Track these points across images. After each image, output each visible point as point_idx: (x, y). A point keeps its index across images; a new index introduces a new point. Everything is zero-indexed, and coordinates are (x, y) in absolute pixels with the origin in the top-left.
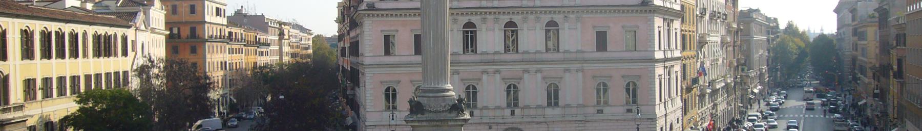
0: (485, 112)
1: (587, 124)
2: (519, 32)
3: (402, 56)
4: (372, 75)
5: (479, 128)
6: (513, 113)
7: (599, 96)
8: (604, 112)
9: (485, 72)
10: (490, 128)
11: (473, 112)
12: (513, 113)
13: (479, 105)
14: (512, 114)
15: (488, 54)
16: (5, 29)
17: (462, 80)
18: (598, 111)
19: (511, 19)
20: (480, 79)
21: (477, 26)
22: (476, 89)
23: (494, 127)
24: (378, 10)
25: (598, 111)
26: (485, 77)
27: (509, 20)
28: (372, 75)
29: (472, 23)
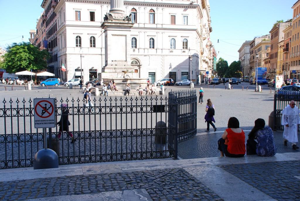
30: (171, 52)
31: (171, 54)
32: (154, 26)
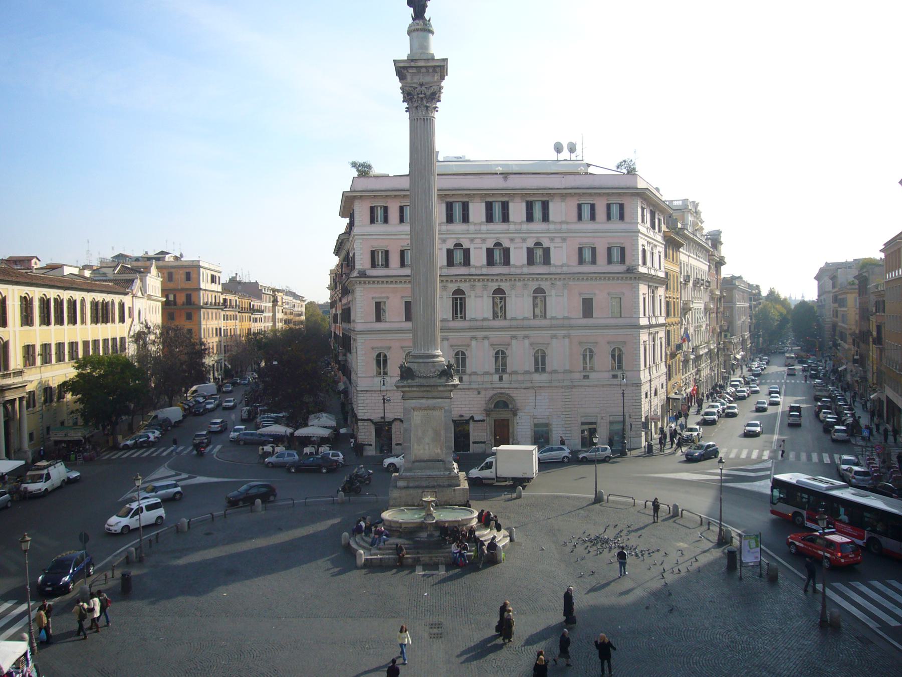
0: (474, 378)
1: (574, 390)
2: (507, 299)
4: (363, 341)
8: (590, 377)
10: (479, 393)
12: (501, 379)
13: (468, 370)
15: (476, 320)
17: (451, 346)
18: (584, 376)
22: (465, 355)
23: (483, 392)
25: (584, 376)
26: (474, 343)
27: (497, 287)
30: (586, 377)
31: (586, 382)
32: (544, 322)
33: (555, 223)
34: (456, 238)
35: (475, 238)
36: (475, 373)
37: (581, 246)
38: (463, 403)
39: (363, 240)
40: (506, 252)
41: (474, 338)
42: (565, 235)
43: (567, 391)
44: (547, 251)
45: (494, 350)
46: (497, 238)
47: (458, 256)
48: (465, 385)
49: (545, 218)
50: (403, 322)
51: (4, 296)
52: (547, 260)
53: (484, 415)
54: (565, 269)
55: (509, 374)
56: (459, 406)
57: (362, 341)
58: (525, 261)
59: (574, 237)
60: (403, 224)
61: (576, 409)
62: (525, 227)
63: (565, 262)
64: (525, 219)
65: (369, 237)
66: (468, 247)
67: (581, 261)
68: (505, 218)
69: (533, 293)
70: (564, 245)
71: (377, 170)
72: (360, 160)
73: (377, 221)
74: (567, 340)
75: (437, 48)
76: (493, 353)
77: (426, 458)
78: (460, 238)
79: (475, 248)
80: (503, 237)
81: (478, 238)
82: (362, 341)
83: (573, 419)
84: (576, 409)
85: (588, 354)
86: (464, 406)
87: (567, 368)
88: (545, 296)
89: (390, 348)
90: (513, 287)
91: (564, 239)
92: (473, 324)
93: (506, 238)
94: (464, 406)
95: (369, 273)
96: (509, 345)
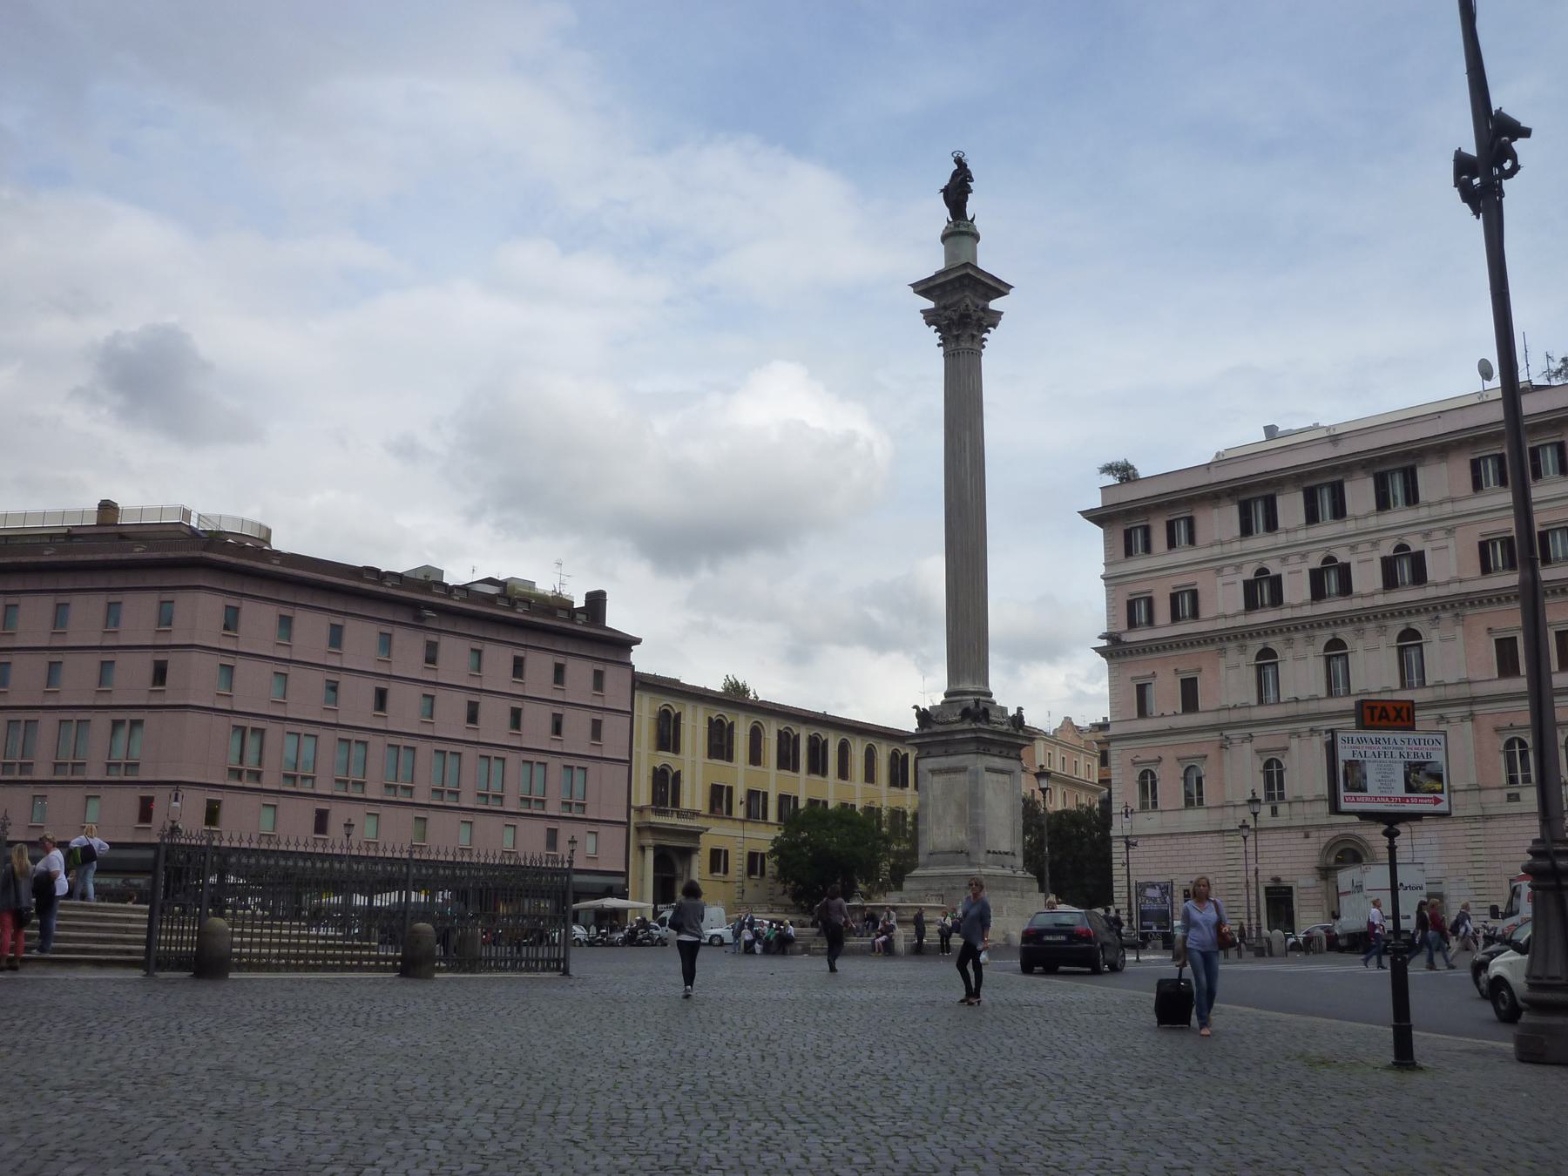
0: (1297, 807)
1: (1490, 824)
2: (1280, 665)
3: (531, 779)
4: (1120, 752)
5: (1288, 835)
6: (1274, 812)
7: (1511, 767)
8: (1521, 797)
9: (1295, 733)
10: (1307, 836)
11: (1276, 808)
12: (1274, 812)
13: (1288, 795)
14: (1272, 814)
15: (1445, 685)
16: (680, 713)
17: (1258, 752)
18: (1509, 795)
19: (1407, 624)
20: (1286, 749)
21: (1422, 633)
22: (1282, 766)
23: (1314, 834)
24: (1125, 643)
25: (1509, 795)
26: (1294, 743)
27: (1331, 638)
28: (1120, 752)
29: (1414, 630)
33: (1429, 505)
34: (1256, 560)
35: (1359, 543)
36: (1300, 800)
37: (1544, 529)
38: (1146, 854)
39: (1117, 585)
40: (1345, 572)
41: (1296, 734)
42: (1450, 523)
43: (1474, 826)
44: (1418, 561)
45: (1261, 759)
46: (1400, 537)
47: (1405, 570)
48: (1281, 821)
49: (1412, 498)
50: (1495, 679)
51: (730, 722)
52: (1419, 577)
53: (1318, 877)
54: (1455, 589)
55: (1290, 803)
56: (1273, 861)
57: (1117, 752)
58: (1378, 583)
59: (1467, 524)
60: (1174, 550)
61: (1497, 864)
62: (1237, 547)
63: (1454, 574)
64: (1374, 507)
65: (1168, 572)
66: (1421, 549)
67: (1486, 569)
68: (1339, 512)
69: (1398, 641)
70: (1451, 542)
71: (1282, 427)
72: (1117, 457)
73: (1137, 551)
74: (1468, 725)
75: (988, 260)
76: (1260, 765)
77: (947, 847)
78: (1263, 559)
79: (1289, 573)
80: (1268, 559)
81: (1293, 554)
82: (1117, 752)
83: (1492, 885)
84: (1497, 864)
85: (1517, 750)
86: (1281, 860)
87: (1473, 780)
88: (1421, 643)
89: (1206, 756)
90: (1289, 642)
91: (1450, 531)
92: (1441, 693)
93: (1272, 558)
94: (1281, 860)
95: (1125, 638)
96: (1286, 749)
